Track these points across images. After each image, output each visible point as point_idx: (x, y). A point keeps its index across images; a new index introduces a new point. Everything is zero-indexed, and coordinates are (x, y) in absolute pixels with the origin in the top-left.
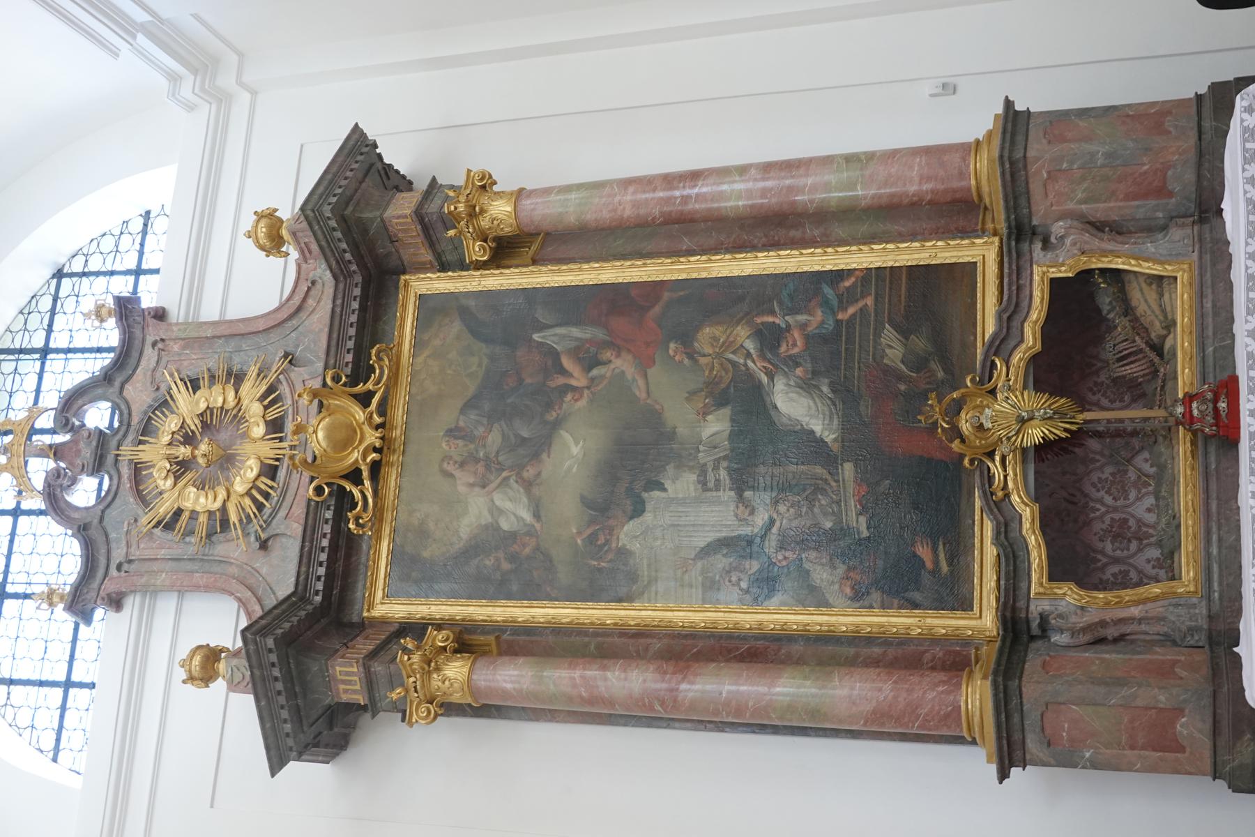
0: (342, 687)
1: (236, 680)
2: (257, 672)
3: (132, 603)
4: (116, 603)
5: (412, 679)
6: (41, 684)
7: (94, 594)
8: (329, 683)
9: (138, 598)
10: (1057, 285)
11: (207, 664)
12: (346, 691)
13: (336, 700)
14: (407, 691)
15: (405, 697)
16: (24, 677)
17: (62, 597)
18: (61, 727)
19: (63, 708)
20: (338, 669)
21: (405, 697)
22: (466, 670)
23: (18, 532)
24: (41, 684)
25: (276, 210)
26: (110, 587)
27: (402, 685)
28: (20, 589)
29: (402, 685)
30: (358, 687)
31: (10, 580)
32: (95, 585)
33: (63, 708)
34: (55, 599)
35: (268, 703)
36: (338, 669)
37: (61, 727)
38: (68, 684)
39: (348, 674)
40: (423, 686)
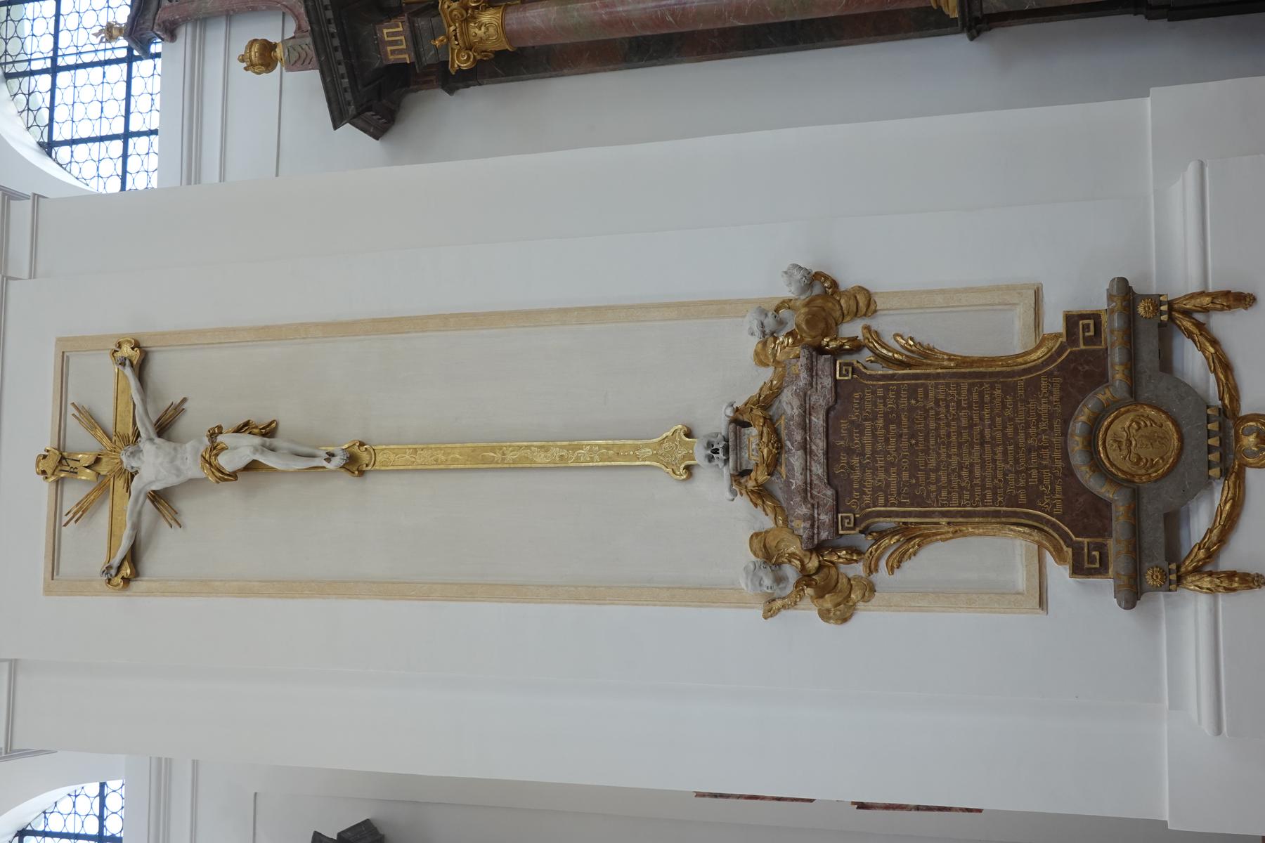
0: (389, 48)
1: (293, 59)
2: (316, 28)
3: (185, 33)
4: (171, 33)
5: (452, 28)
6: (101, 139)
7: (149, 24)
8: (379, 44)
9: (189, 29)
10: (1108, 505)
11: (264, 57)
12: (393, 52)
13: (385, 63)
14: (449, 39)
15: (447, 45)
16: (85, 136)
17: (120, 30)
18: (125, 171)
19: (125, 156)
20: (385, 31)
21: (447, 45)
22: (499, 15)
23: (62, 12)
24: (101, 139)
25: (246, 69)
26: (163, 15)
27: (444, 33)
28: (71, 60)
29: (444, 33)
30: (404, 46)
31: (60, 53)
32: (149, 16)
33: (125, 156)
34: (115, 33)
35: (327, 57)
36: (385, 31)
37: (125, 171)
38: (127, 136)
39: (394, 34)
40: (462, 33)
